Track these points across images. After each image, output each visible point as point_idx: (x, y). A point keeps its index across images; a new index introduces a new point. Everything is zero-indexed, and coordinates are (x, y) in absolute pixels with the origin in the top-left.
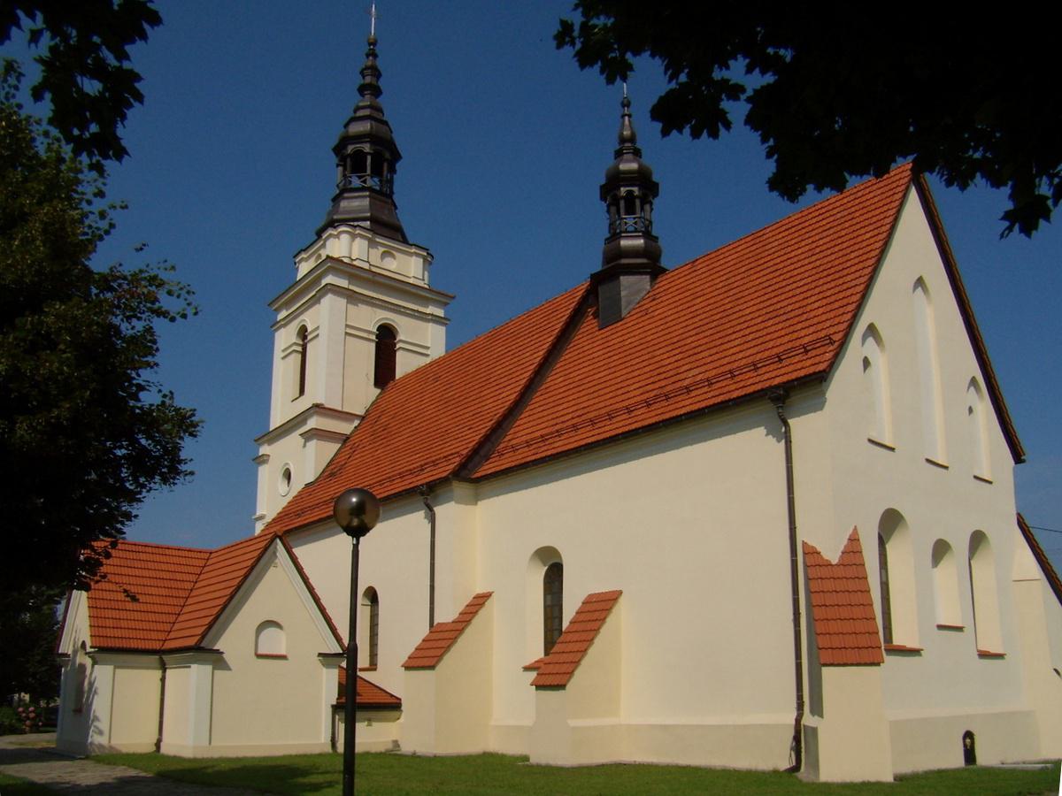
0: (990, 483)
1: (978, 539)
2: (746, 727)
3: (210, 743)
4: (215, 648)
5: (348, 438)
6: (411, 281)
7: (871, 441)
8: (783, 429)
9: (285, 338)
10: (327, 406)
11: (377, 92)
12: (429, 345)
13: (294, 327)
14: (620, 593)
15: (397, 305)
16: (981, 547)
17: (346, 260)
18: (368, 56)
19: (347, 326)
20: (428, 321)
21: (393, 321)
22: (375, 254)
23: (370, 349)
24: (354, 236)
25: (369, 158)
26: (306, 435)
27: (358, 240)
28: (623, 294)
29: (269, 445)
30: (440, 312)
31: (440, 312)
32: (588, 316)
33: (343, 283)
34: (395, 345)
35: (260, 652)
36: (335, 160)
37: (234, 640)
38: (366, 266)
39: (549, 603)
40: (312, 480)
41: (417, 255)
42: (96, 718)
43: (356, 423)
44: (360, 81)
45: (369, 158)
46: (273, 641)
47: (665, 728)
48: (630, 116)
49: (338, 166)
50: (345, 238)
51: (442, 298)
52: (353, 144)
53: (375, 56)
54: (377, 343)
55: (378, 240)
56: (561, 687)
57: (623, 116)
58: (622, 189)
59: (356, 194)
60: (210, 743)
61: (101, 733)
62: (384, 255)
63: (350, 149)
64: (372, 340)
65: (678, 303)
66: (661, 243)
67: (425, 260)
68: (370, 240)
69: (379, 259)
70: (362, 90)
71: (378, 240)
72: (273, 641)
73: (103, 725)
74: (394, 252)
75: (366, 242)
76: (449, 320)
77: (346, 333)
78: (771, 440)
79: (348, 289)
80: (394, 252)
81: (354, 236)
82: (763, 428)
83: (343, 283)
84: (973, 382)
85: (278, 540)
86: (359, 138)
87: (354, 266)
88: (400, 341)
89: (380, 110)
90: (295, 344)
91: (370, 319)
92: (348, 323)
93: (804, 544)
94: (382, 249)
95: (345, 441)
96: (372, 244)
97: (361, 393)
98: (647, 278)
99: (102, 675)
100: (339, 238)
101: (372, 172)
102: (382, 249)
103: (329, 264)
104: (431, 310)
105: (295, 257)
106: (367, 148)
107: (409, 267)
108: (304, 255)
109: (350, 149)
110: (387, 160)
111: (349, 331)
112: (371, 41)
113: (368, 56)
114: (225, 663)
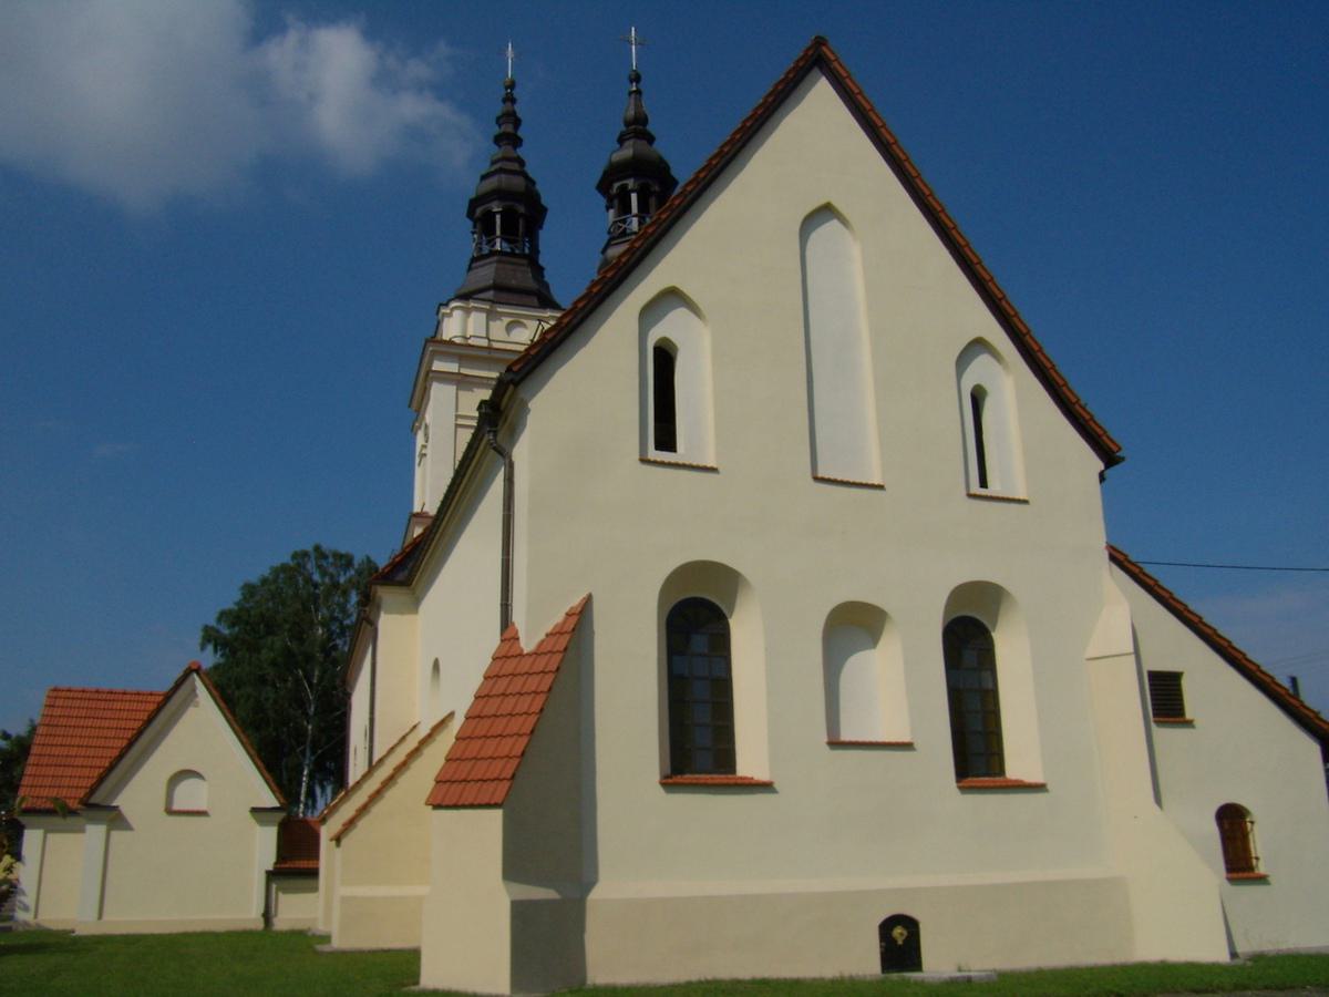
3: (100, 916)
4: (114, 804)
11: (516, 142)
16: (1002, 611)
17: (457, 340)
19: (457, 417)
22: (498, 330)
24: (467, 311)
25: (498, 217)
27: (474, 315)
35: (176, 807)
36: (602, 201)
37: (139, 794)
39: (987, 674)
42: (24, 893)
45: (498, 217)
46: (187, 797)
49: (608, 209)
52: (618, 180)
53: (513, 101)
55: (499, 310)
60: (100, 916)
61: (26, 908)
62: (509, 328)
69: (505, 333)
71: (499, 310)
72: (187, 797)
73: (29, 899)
77: (457, 426)
79: (459, 374)
81: (467, 311)
85: (195, 675)
89: (521, 162)
92: (459, 413)
94: (507, 320)
101: (502, 233)
102: (507, 320)
109: (479, 211)
110: (522, 215)
111: (460, 422)
112: (507, 84)
113: (504, 101)
114: (126, 821)
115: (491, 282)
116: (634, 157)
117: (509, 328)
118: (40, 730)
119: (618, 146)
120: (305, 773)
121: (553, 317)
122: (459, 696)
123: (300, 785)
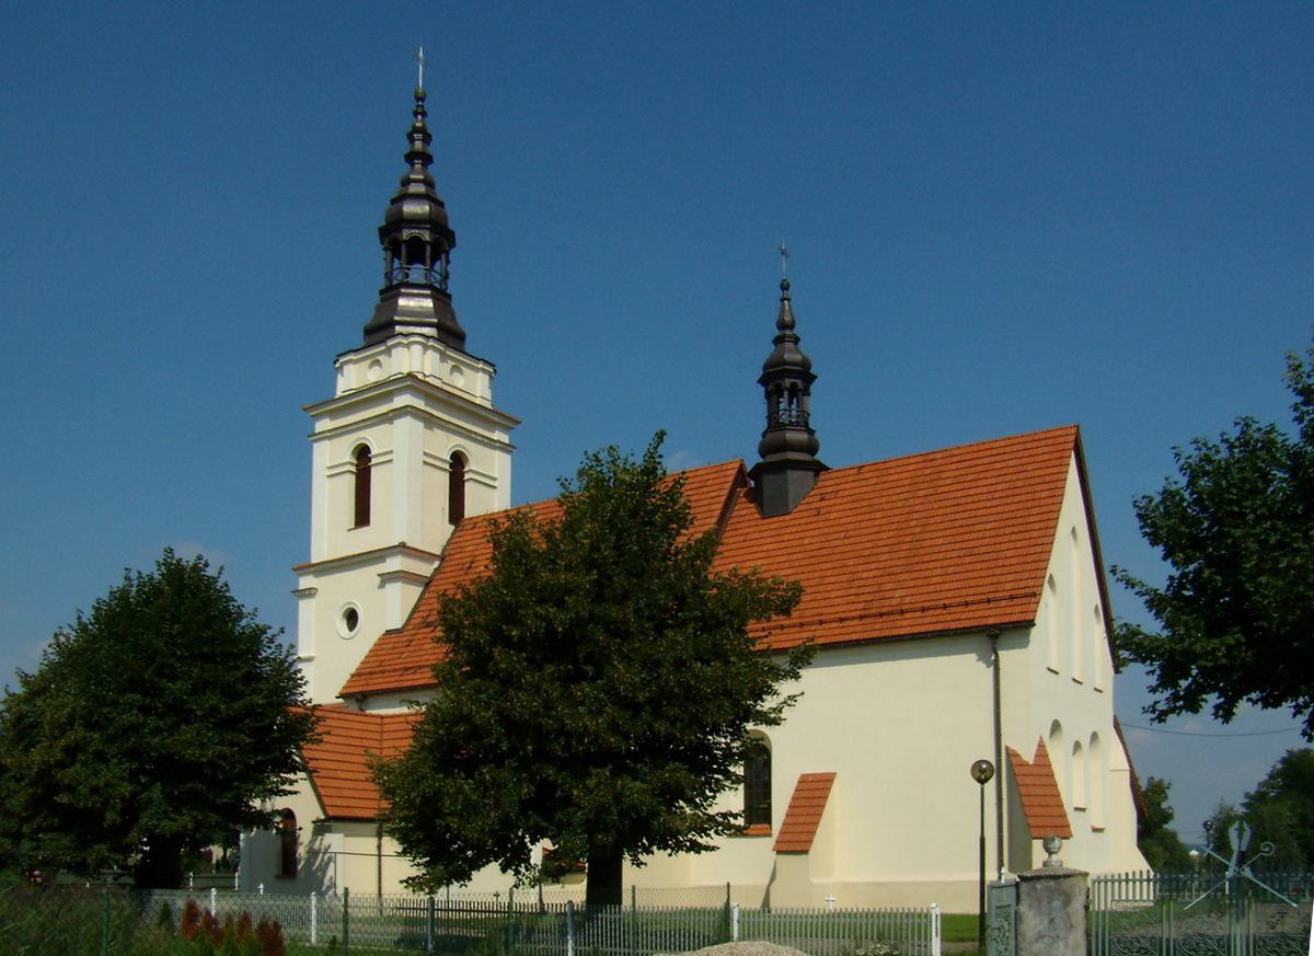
0: (1081, 683)
1: (1094, 736)
2: (954, 883)
5: (430, 582)
6: (478, 401)
7: (1049, 669)
8: (993, 657)
9: (330, 457)
10: (409, 544)
11: (427, 159)
12: (496, 476)
13: (346, 446)
14: (835, 774)
15: (468, 430)
17: (420, 376)
18: (416, 114)
20: (495, 448)
21: (464, 448)
23: (445, 479)
25: (428, 248)
26: (385, 578)
27: (430, 352)
28: (790, 487)
29: (316, 576)
30: (505, 438)
31: (505, 438)
32: (739, 497)
33: (420, 404)
34: (463, 474)
38: (437, 383)
40: (400, 627)
41: (484, 371)
43: (436, 564)
44: (407, 148)
45: (428, 248)
47: (880, 885)
48: (789, 300)
50: (417, 349)
51: (508, 422)
53: (424, 114)
54: (450, 473)
55: (448, 353)
56: (806, 852)
57: (783, 300)
58: (786, 380)
59: (415, 291)
62: (455, 369)
63: (406, 234)
64: (444, 470)
65: (858, 511)
66: (817, 435)
67: (491, 378)
68: (442, 354)
70: (410, 158)
71: (448, 353)
74: (462, 367)
75: (487, 377)
76: (514, 448)
78: (982, 665)
80: (462, 367)
81: (426, 347)
82: (974, 655)
83: (420, 404)
84: (1097, 608)
86: (415, 221)
87: (428, 383)
88: (470, 471)
90: (350, 463)
91: (444, 445)
93: (1007, 748)
95: (427, 585)
96: (444, 357)
97: (435, 533)
98: (811, 473)
99: (334, 840)
100: (409, 349)
103: (409, 383)
104: (498, 435)
105: (339, 356)
106: (427, 236)
107: (475, 385)
108: (352, 357)
109: (406, 234)
112: (420, 95)
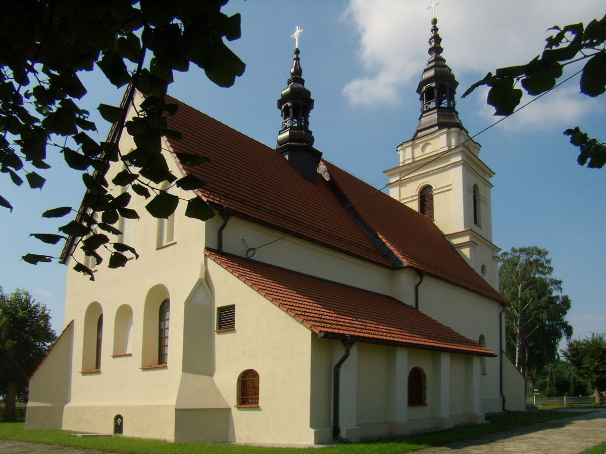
24: (404, 149)
55: (417, 142)
62: (423, 149)
71: (417, 142)
94: (421, 145)
102: (421, 145)
115: (437, 122)
116: (519, 348)
117: (423, 149)
118: (75, 438)
119: (96, 131)
120: (517, 350)
121: (586, 364)
122: (191, 191)
123: (518, 358)
